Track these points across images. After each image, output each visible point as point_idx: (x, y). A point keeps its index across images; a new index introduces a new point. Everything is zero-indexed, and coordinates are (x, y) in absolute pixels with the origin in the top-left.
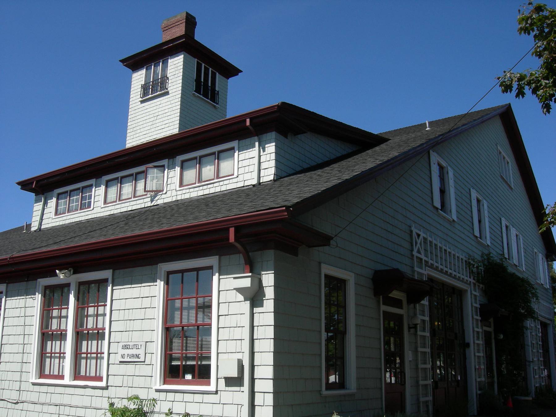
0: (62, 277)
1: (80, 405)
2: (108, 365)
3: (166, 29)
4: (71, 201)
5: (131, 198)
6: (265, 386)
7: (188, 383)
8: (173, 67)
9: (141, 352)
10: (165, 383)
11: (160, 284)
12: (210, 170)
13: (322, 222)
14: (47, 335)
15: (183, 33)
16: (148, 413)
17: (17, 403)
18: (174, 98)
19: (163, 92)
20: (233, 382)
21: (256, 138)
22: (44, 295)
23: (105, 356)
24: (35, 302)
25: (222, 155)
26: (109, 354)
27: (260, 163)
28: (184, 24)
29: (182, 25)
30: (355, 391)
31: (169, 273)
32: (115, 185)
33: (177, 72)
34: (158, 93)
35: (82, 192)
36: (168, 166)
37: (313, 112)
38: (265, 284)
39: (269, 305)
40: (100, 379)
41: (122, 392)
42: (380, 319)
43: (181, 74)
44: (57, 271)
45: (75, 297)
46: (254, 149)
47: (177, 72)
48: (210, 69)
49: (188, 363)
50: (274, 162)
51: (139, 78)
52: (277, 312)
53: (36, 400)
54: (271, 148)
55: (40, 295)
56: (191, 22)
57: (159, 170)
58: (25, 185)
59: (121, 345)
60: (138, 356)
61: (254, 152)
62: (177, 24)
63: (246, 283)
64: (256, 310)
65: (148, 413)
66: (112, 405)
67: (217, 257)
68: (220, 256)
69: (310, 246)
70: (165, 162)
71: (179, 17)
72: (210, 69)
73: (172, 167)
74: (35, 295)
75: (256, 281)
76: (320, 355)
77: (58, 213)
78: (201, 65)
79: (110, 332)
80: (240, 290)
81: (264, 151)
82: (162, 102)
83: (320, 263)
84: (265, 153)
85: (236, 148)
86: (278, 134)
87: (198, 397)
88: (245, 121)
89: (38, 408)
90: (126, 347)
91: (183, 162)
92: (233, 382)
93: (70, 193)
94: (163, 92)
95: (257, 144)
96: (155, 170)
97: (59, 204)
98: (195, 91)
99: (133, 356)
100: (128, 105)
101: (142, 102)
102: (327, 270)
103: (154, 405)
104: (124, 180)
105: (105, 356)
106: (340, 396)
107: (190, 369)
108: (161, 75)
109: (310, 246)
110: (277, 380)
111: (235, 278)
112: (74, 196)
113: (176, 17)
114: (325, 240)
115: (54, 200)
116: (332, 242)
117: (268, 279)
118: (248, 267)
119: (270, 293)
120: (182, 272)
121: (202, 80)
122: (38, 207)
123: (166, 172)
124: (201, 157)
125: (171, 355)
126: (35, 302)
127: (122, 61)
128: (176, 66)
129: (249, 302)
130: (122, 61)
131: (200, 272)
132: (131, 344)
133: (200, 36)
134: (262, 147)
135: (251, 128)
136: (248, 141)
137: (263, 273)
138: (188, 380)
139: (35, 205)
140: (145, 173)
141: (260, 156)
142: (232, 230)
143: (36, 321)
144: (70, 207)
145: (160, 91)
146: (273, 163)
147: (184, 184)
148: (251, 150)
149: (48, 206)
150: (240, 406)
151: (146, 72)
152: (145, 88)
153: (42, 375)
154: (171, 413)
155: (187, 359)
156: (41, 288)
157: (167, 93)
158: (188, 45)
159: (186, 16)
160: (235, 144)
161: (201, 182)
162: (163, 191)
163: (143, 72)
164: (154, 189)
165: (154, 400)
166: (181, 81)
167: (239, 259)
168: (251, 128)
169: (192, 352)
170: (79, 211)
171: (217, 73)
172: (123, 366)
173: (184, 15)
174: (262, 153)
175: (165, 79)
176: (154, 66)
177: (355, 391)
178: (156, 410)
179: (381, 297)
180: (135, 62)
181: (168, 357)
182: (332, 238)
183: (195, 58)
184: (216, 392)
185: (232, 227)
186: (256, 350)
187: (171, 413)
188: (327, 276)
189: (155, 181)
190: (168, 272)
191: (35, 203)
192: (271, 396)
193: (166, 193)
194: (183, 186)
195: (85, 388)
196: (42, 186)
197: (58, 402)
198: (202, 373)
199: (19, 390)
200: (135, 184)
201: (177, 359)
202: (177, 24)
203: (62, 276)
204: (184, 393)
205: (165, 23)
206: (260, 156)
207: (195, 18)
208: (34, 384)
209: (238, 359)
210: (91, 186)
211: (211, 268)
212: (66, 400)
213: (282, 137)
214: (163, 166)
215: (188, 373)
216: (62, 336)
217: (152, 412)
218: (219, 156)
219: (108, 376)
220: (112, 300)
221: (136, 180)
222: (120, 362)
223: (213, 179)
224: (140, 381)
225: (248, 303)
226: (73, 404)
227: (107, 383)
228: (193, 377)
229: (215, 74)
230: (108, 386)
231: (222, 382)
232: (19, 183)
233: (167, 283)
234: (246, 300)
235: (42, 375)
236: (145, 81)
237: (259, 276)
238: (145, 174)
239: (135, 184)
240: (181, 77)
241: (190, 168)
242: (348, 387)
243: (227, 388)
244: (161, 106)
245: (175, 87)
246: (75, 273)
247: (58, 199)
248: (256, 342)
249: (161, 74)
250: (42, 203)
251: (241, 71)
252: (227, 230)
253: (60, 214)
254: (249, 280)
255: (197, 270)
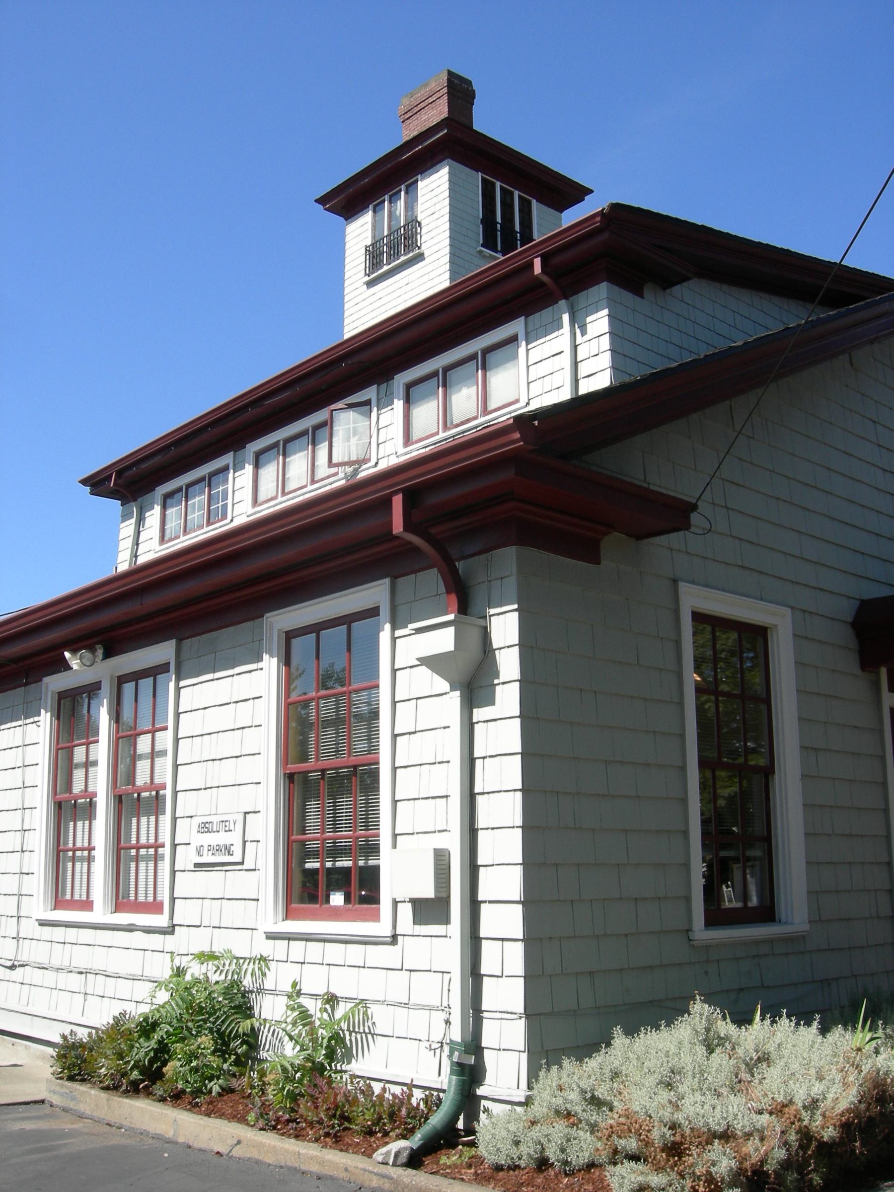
0: (75, 667)
1: (123, 973)
2: (173, 873)
3: (408, 116)
4: (189, 509)
5: (306, 486)
6: (504, 921)
7: (336, 914)
8: (428, 197)
9: (234, 838)
10: (289, 915)
11: (270, 665)
12: (469, 397)
13: (663, 464)
14: (68, 808)
15: (445, 114)
16: (252, 992)
17: (12, 967)
18: (436, 264)
19: (411, 254)
20: (430, 910)
21: (563, 303)
22: (58, 715)
23: (166, 851)
24: (39, 730)
25: (492, 357)
26: (174, 846)
27: (575, 364)
28: (446, 97)
29: (440, 101)
30: (806, 927)
31: (290, 636)
32: (274, 460)
33: (438, 207)
34: (403, 258)
35: (209, 486)
36: (378, 400)
37: (703, 226)
38: (497, 641)
39: (508, 698)
40: (155, 907)
41: (199, 941)
42: (881, 731)
43: (447, 209)
44: (67, 655)
45: (109, 714)
46: (561, 332)
47: (438, 207)
48: (498, 184)
49: (339, 864)
50: (608, 355)
51: (360, 232)
52: (530, 716)
53: (45, 961)
54: (599, 323)
55: (49, 714)
56: (460, 92)
57: (361, 414)
58: (97, 484)
59: (196, 821)
60: (228, 850)
61: (560, 340)
62: (431, 100)
63: (444, 640)
64: (479, 714)
65: (252, 992)
66: (179, 972)
67: (387, 581)
68: (395, 577)
69: (641, 535)
70: (370, 393)
71: (433, 86)
72: (516, 193)
73: (385, 402)
74: (39, 715)
75: (474, 636)
76: (685, 833)
77: (166, 539)
78: (493, 185)
79: (175, 793)
80: (432, 662)
81: (584, 333)
82: (412, 278)
83: (675, 581)
84: (586, 338)
85: (522, 336)
86: (616, 289)
87: (355, 953)
88: (531, 265)
89: (49, 977)
90: (205, 828)
91: (409, 387)
92: (430, 910)
93: (186, 492)
94: (411, 254)
95: (566, 318)
96: (351, 415)
97: (168, 518)
98: (482, 246)
99: (218, 849)
100: (342, 296)
101: (370, 284)
102: (695, 598)
103: (264, 975)
104: (290, 446)
105: (166, 851)
106: (757, 942)
107: (340, 879)
108: (406, 220)
109: (640, 536)
110: (533, 902)
111: (419, 631)
112: (194, 497)
113: (426, 85)
114: (675, 515)
115: (157, 509)
116: (694, 518)
117: (505, 626)
118: (453, 598)
119: (509, 664)
120: (317, 628)
121: (499, 220)
122: (127, 529)
123: (374, 414)
124: (447, 369)
125: (303, 843)
126: (39, 730)
127: (322, 201)
128: (434, 194)
129: (458, 693)
130: (322, 201)
131: (354, 625)
132: (215, 819)
133: (486, 121)
134: (578, 323)
135: (545, 279)
136: (546, 314)
137: (493, 611)
138: (336, 908)
139: (122, 525)
140: (327, 424)
141: (575, 347)
142: (398, 502)
143: (40, 777)
144: (188, 522)
145: (405, 254)
146: (606, 360)
147: (415, 438)
148: (555, 334)
149: (146, 525)
150: (447, 976)
151: (374, 217)
152: (374, 257)
153: (59, 903)
154: (299, 993)
155: (336, 852)
156: (49, 699)
157: (420, 257)
158: (456, 140)
159: (449, 80)
160: (516, 326)
161: (450, 429)
162: (369, 460)
163: (366, 220)
164: (354, 458)
165: (263, 959)
166: (447, 225)
167: (432, 580)
168: (545, 279)
169: (345, 835)
170: (205, 529)
171: (534, 202)
172: (202, 875)
173: (444, 77)
174: (579, 339)
175: (413, 224)
176: (390, 202)
177: (806, 927)
178: (269, 984)
179: (883, 671)
180: (349, 199)
181: (294, 848)
182: (694, 507)
183: (478, 171)
184: (394, 939)
185: (396, 493)
186: (481, 822)
187: (299, 993)
188: (698, 617)
189: (354, 441)
190: (287, 633)
191: (123, 522)
192: (520, 947)
193: (377, 463)
194: (412, 444)
195: (131, 931)
196: (130, 482)
197: (83, 965)
198: (364, 888)
199: (17, 938)
200: (314, 452)
201: (315, 854)
202: (431, 100)
203: (75, 664)
204: (324, 941)
205: (405, 103)
206: (575, 347)
207: (469, 83)
208: (43, 923)
209: (435, 850)
210: (226, 469)
211: (373, 612)
212: (97, 959)
213: (627, 297)
214: (368, 403)
215: (338, 889)
216: (89, 811)
217: (260, 991)
218: (484, 361)
219: (173, 899)
220: (177, 715)
221: (314, 444)
222: (197, 865)
223: (475, 418)
224: (234, 913)
225: (455, 698)
226: (111, 970)
227: (172, 917)
228: (347, 900)
229: (529, 202)
230: (174, 926)
231: (406, 912)
232: (84, 482)
233: (287, 660)
234: (453, 689)
235: (59, 903)
236: (374, 237)
237: (481, 622)
238: (327, 428)
239: (314, 452)
240: (447, 217)
241: (424, 397)
242: (783, 919)
243: (417, 927)
244: (409, 287)
245: (435, 240)
246: (108, 655)
247: (164, 507)
248: (480, 800)
249: (406, 216)
250: (133, 521)
251: (591, 191)
252: (386, 503)
253: (171, 540)
254: (449, 633)
255: (348, 620)
